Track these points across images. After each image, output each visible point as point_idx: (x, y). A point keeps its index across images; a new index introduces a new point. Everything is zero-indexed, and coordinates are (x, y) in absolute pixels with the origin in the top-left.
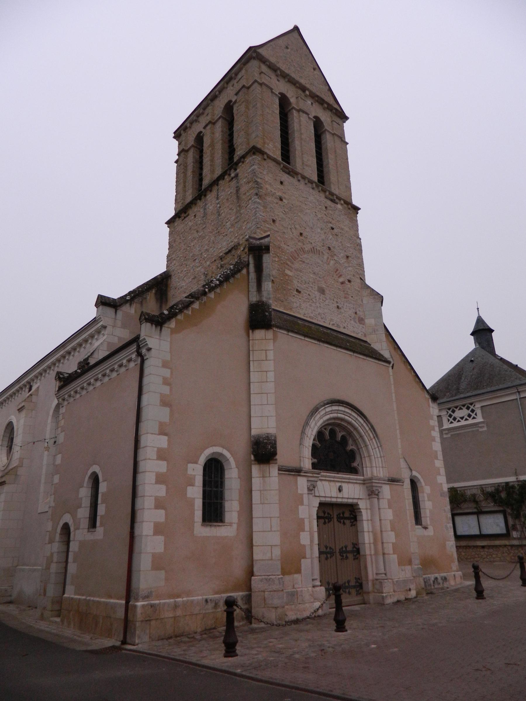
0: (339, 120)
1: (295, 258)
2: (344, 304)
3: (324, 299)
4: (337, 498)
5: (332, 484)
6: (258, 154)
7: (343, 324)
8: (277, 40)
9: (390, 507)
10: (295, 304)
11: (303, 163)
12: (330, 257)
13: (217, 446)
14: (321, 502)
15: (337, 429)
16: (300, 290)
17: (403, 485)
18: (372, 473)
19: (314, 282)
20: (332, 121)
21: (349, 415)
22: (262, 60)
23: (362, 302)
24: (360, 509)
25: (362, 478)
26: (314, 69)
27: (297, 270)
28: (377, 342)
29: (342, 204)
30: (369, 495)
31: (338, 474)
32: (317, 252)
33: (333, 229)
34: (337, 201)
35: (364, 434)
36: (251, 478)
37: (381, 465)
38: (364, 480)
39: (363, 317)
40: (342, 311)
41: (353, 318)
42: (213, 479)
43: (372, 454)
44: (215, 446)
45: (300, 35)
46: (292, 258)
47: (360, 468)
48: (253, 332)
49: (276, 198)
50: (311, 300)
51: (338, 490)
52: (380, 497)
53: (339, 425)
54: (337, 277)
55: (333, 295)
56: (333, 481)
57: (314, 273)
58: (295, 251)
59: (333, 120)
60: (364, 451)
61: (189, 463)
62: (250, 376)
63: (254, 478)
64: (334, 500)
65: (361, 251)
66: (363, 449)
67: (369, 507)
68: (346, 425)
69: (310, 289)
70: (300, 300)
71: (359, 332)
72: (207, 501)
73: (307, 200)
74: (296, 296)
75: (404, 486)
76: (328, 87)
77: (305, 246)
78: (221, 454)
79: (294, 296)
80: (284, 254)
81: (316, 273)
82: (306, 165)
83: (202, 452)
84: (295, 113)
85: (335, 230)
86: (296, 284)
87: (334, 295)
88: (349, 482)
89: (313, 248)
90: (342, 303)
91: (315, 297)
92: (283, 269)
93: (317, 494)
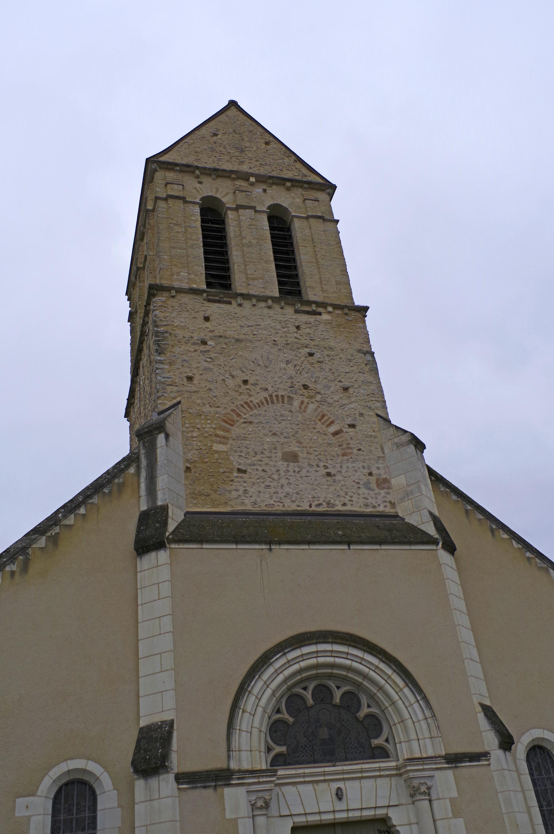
0: (322, 196)
1: (233, 421)
2: (341, 467)
3: (297, 469)
4: (334, 812)
5: (323, 786)
6: (160, 292)
7: (342, 499)
8: (197, 132)
9: (456, 814)
10: (234, 493)
11: (247, 278)
12: (306, 400)
13: (75, 758)
14: (295, 825)
15: (332, 684)
16: (243, 468)
17: (489, 765)
18: (411, 750)
19: (275, 448)
20: (304, 201)
21: (345, 656)
22: (170, 166)
23: (383, 453)
24: (395, 826)
25: (394, 764)
26: (267, 143)
27: (238, 438)
28: (414, 512)
29: (330, 312)
30: (412, 796)
31: (334, 766)
32: (278, 400)
33: (311, 355)
34: (320, 310)
35: (383, 682)
36: (132, 803)
37: (427, 735)
38: (397, 768)
39: (388, 477)
40: (339, 477)
41: (364, 484)
42: (75, 816)
43: (407, 716)
44: (72, 759)
45: (240, 111)
46: (227, 422)
47: (390, 747)
48: (141, 558)
49: (194, 344)
50: (269, 477)
51: (334, 797)
52: (434, 797)
53: (330, 676)
54: (324, 426)
55: (316, 458)
56: (325, 781)
57: (275, 434)
58: (233, 410)
59: (306, 198)
60: (392, 713)
61: (18, 797)
62: (137, 629)
63: (137, 804)
64: (328, 817)
65: (375, 370)
66: (390, 709)
67: (413, 820)
68: (345, 673)
69: (266, 460)
70: (245, 484)
71: (380, 502)
72: (545, 776)
73: (259, 327)
74: (236, 479)
75: (491, 766)
76: (293, 157)
77: (252, 399)
78: (85, 771)
79: (232, 481)
80: (209, 422)
81: (278, 433)
82: (254, 279)
83: (47, 774)
84: (231, 215)
85: (317, 355)
86: (236, 461)
87: (319, 456)
88: (362, 778)
89: (271, 396)
90: (338, 465)
91: (278, 471)
92: (209, 445)
93: (285, 812)
